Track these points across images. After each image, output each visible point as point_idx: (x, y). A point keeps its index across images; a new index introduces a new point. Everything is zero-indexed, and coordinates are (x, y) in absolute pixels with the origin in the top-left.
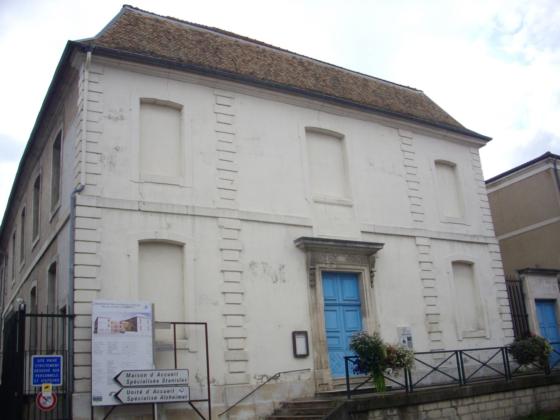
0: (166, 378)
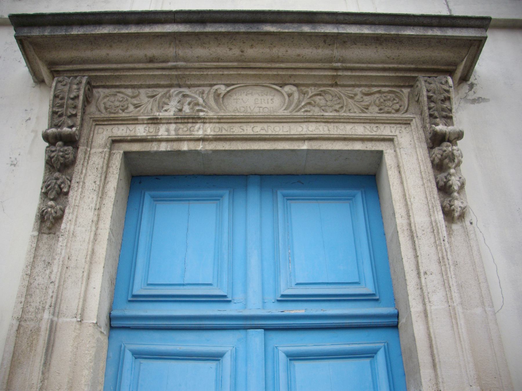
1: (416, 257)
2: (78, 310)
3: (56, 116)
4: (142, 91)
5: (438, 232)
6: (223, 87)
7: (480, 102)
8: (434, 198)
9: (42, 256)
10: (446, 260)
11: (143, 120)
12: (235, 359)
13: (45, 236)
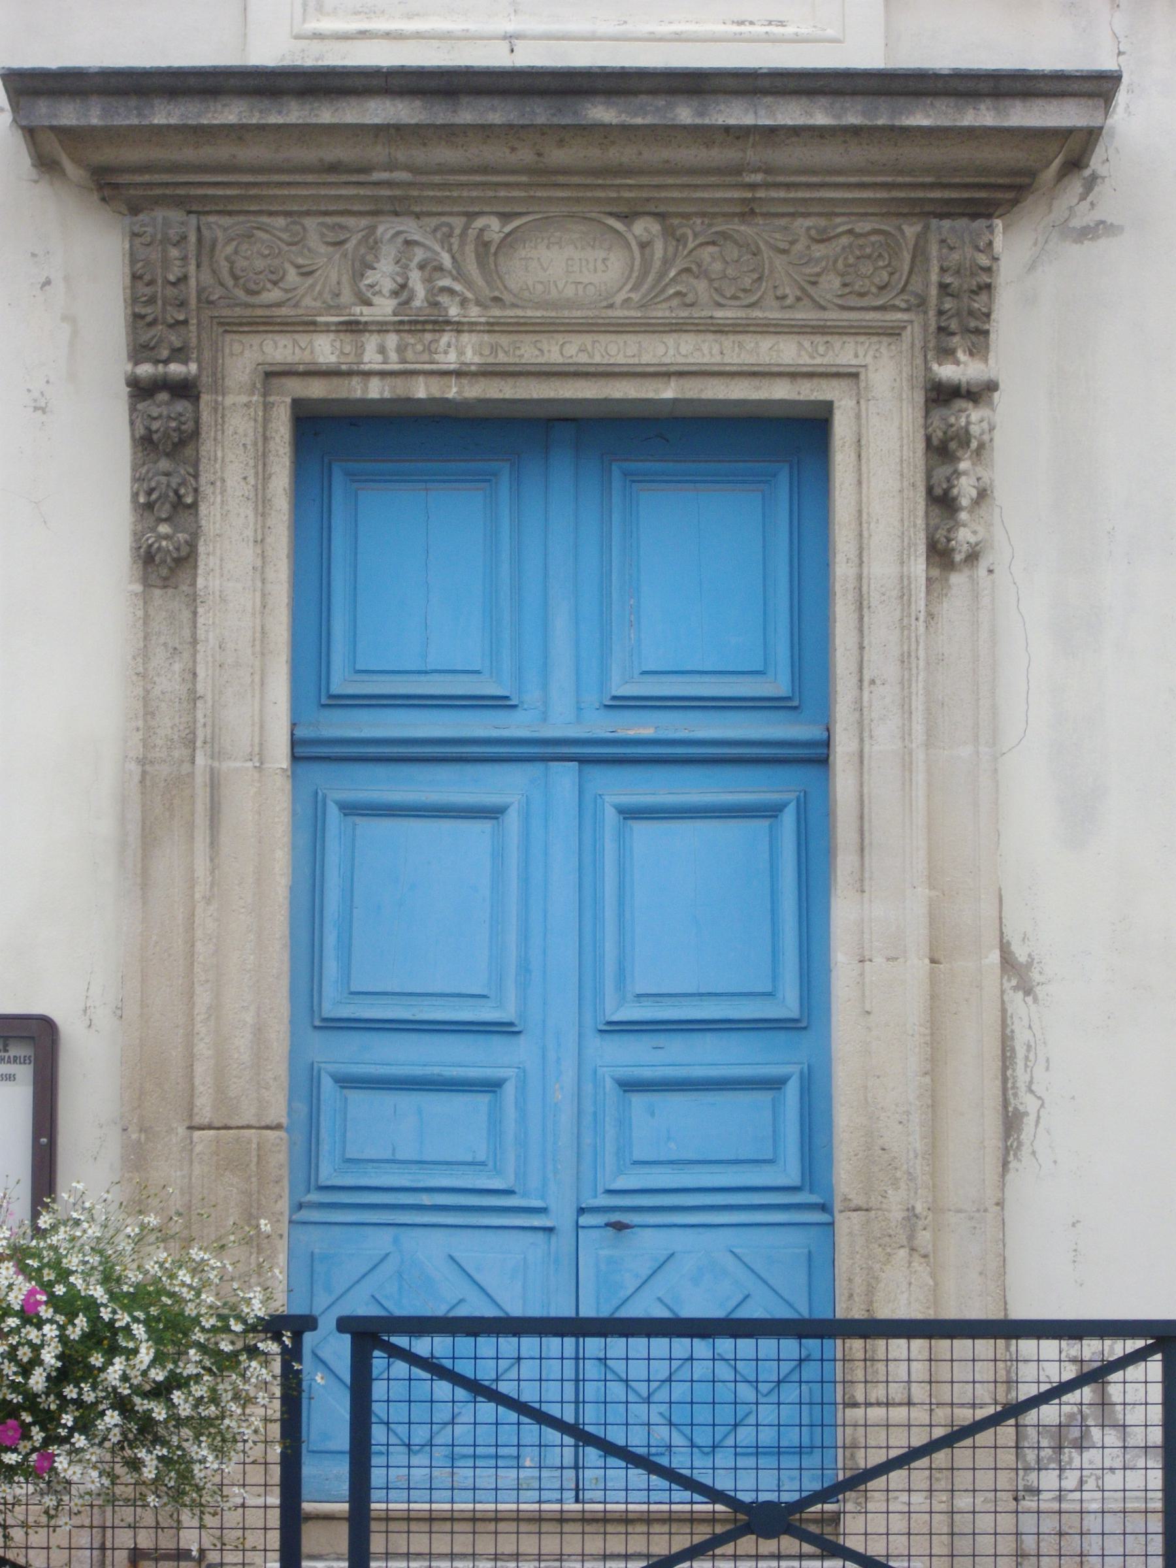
0: (680, 1391)
1: (862, 648)
2: (252, 745)
3: (141, 323)
4: (310, 223)
5: (909, 600)
6: (494, 223)
7: (1099, 237)
8: (915, 526)
9: (159, 634)
10: (913, 659)
11: (327, 324)
12: (526, 817)
13: (157, 592)
